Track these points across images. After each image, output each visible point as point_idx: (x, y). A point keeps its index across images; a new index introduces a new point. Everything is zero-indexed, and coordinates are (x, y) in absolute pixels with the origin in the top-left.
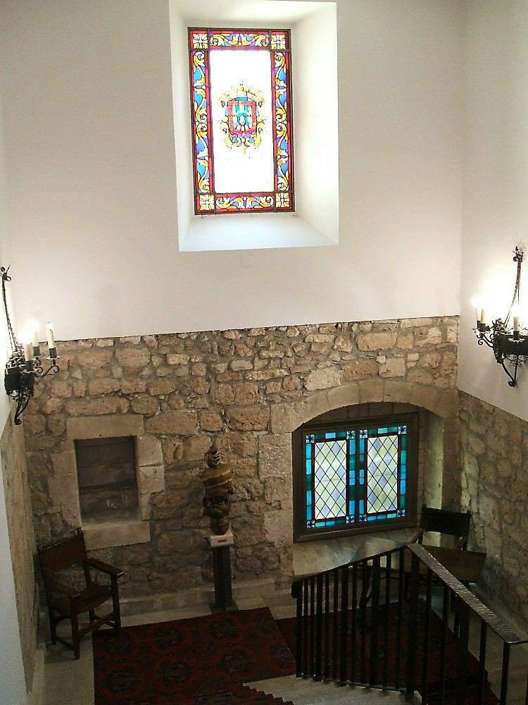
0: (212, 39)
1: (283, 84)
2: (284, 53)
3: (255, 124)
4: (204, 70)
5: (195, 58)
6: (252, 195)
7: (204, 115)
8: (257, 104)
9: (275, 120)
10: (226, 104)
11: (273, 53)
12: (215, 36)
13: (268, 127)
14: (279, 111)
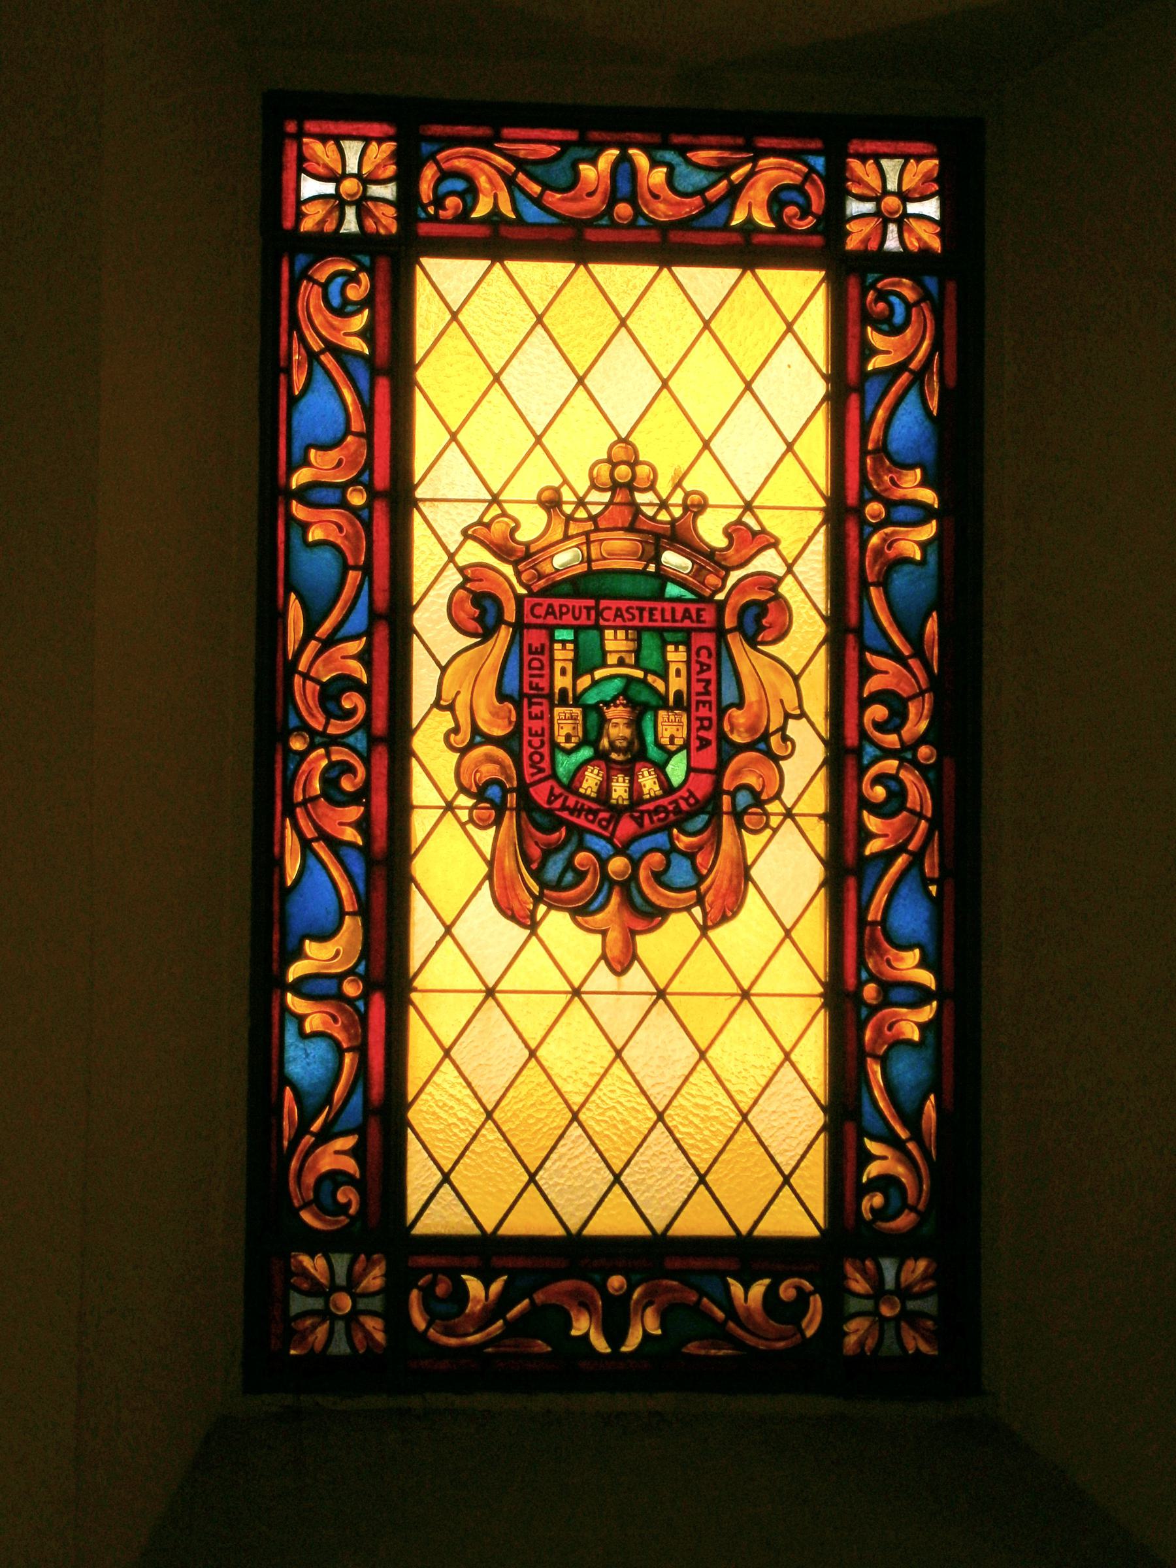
0: (429, 173)
1: (914, 487)
2: (931, 283)
3: (708, 758)
4: (358, 869)
5: (310, 296)
6: (510, 913)
7: (347, 683)
8: (729, 622)
9: (851, 738)
10: (510, 615)
11: (856, 281)
12: (458, 159)
13: (434, 628)
14: (886, 674)
